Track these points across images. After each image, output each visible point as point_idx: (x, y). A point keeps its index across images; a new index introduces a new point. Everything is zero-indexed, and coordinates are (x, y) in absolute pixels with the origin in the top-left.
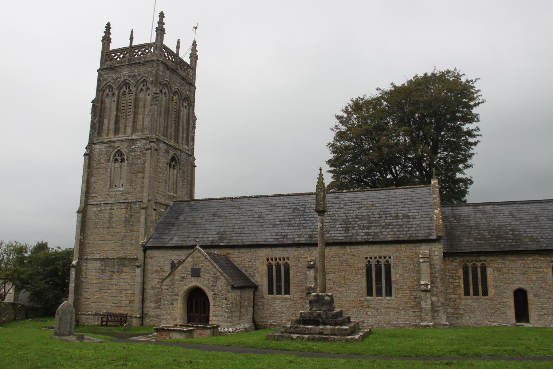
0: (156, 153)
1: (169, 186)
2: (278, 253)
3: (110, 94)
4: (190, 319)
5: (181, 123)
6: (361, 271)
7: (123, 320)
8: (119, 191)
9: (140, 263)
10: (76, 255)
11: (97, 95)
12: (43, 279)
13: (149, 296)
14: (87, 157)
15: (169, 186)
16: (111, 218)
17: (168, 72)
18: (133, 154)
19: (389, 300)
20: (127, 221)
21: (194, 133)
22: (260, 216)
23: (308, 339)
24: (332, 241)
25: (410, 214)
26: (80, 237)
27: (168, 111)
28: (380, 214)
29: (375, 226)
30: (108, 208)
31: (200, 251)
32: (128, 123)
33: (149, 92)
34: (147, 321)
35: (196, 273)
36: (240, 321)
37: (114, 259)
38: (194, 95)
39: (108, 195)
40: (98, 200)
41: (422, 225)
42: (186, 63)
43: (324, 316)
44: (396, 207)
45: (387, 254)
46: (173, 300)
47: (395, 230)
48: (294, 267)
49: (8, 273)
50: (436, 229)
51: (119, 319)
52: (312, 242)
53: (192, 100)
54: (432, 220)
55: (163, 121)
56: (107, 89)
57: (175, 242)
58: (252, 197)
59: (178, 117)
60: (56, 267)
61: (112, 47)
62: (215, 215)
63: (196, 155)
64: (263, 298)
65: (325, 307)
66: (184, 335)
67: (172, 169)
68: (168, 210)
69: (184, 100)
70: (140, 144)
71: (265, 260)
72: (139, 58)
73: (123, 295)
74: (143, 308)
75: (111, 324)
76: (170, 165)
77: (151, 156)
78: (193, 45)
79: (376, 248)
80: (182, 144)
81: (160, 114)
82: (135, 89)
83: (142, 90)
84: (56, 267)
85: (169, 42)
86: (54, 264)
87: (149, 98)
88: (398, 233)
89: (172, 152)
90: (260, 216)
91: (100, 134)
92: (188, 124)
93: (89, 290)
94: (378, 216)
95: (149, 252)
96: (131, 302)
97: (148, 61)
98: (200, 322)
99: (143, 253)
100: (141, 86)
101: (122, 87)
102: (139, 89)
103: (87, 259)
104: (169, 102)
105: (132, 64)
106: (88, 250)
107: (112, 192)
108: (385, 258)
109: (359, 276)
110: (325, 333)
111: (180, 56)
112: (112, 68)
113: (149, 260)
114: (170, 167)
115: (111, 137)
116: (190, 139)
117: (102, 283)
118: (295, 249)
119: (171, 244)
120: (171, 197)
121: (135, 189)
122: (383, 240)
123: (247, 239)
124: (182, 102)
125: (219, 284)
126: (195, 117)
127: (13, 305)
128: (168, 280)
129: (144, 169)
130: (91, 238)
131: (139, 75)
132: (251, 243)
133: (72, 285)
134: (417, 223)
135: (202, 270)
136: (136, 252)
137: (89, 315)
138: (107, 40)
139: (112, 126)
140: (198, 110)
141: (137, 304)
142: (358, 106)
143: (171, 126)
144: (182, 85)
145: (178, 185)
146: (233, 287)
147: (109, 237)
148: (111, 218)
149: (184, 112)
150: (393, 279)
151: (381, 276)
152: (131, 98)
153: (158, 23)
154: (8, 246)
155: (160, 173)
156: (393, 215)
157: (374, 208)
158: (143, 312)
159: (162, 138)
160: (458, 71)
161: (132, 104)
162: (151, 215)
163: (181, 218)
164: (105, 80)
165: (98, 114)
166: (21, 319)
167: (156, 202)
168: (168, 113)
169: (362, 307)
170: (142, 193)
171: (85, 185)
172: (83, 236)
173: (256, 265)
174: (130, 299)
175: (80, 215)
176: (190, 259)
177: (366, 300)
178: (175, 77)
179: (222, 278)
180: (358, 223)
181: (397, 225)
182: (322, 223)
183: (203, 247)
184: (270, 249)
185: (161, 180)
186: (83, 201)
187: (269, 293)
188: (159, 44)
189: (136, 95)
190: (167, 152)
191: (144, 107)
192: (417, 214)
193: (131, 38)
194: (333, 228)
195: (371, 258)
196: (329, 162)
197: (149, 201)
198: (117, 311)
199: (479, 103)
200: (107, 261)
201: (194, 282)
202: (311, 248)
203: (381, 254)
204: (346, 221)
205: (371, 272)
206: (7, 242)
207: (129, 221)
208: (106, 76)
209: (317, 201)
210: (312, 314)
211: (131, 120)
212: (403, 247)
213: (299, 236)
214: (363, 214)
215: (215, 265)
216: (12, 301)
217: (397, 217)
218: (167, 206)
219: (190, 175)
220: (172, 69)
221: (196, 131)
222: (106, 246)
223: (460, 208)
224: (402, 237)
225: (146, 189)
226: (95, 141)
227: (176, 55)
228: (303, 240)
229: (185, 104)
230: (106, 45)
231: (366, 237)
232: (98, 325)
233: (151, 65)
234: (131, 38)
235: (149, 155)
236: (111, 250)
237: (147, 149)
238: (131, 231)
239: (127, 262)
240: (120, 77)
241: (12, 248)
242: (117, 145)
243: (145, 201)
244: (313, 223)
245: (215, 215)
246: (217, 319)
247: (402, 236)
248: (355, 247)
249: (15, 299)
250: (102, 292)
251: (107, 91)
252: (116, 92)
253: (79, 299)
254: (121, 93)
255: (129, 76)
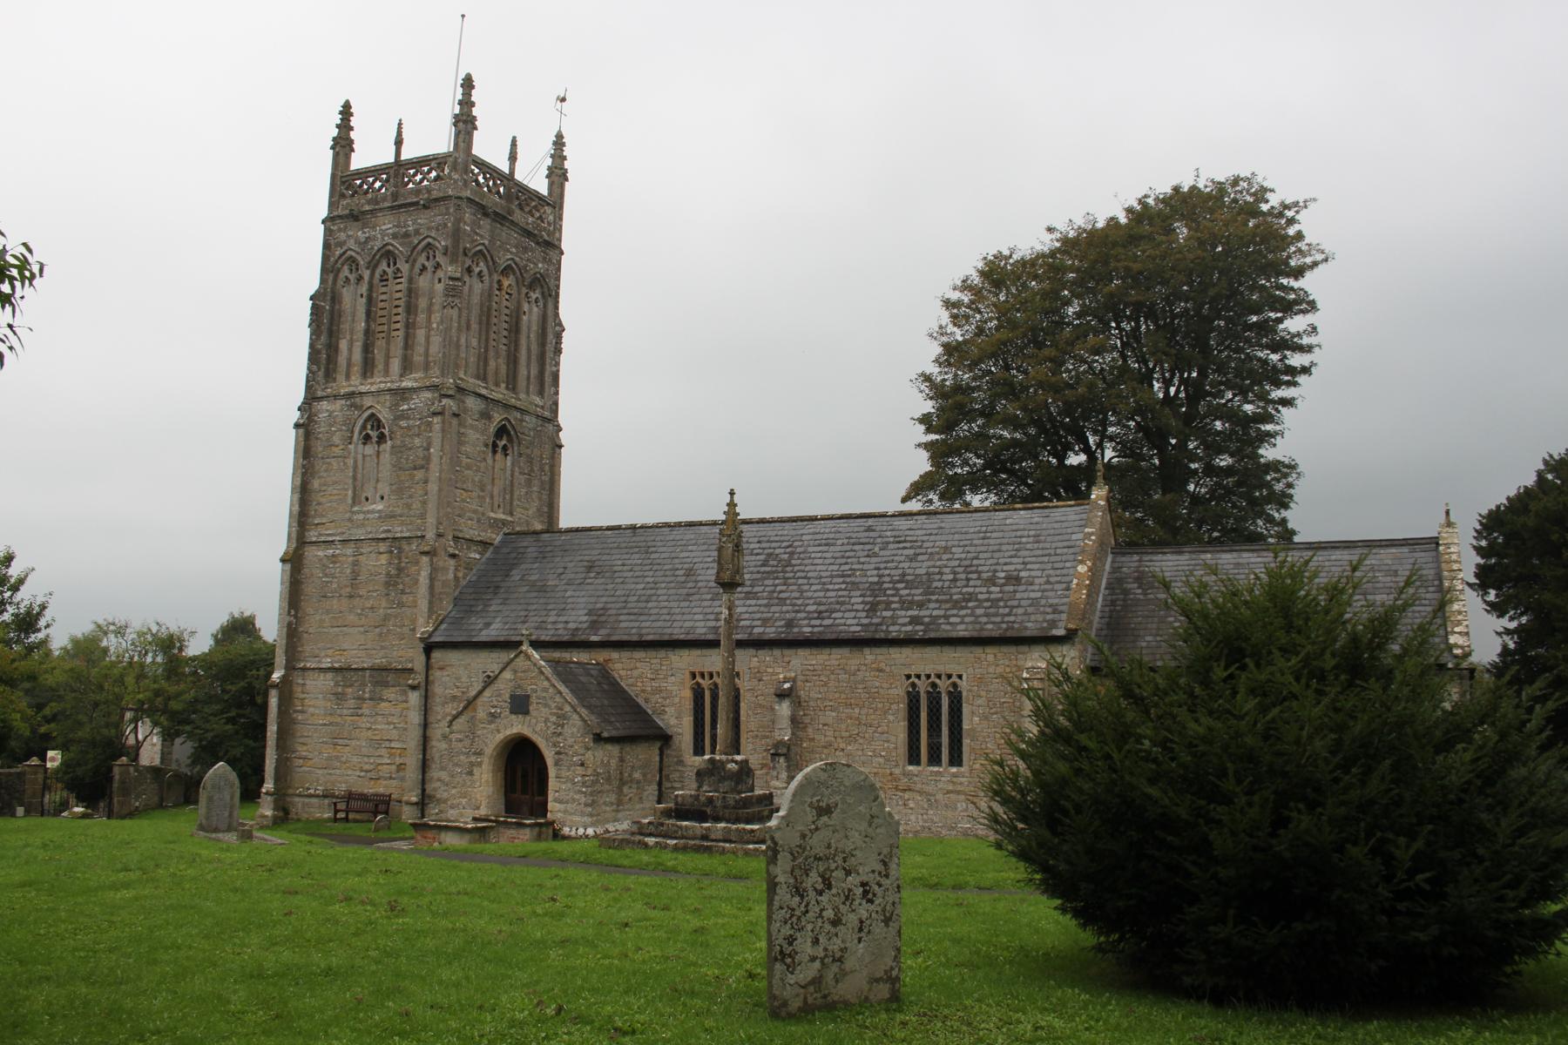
0: (455, 421)
1: (492, 497)
2: (713, 661)
3: (352, 277)
4: (511, 807)
5: (523, 341)
6: (894, 707)
7: (382, 807)
8: (372, 512)
9: (419, 679)
10: (280, 659)
11: (323, 281)
12: (222, 712)
13: (437, 756)
14: (301, 431)
15: (492, 497)
16: (355, 575)
17: (486, 223)
18: (403, 423)
19: (955, 775)
20: (390, 583)
21: (558, 364)
22: (689, 573)
23: (676, 848)
24: (833, 636)
25: (1023, 574)
26: (288, 619)
27: (489, 317)
28: (955, 573)
29: (937, 601)
30: (349, 551)
31: (528, 657)
32: (392, 348)
33: (440, 274)
34: (433, 810)
35: (520, 705)
36: (620, 815)
37: (363, 669)
38: (559, 269)
39: (350, 520)
40: (329, 532)
41: (1043, 602)
42: (536, 195)
43: (719, 803)
44: (996, 555)
45: (953, 669)
46: (472, 764)
47: (979, 611)
48: (748, 695)
49: (141, 696)
50: (1069, 613)
51: (370, 806)
52: (790, 637)
53: (552, 283)
54: (1068, 589)
55: (474, 342)
56: (346, 267)
57: (493, 632)
58: (679, 525)
59: (515, 329)
60: (250, 684)
61: (358, 162)
62: (590, 568)
63: (562, 419)
64: (681, 762)
65: (727, 785)
66: (467, 837)
67: (499, 456)
68: (488, 555)
69: (531, 287)
70: (420, 401)
71: (688, 676)
72: (417, 192)
73: (383, 752)
74: (423, 782)
75: (358, 816)
76: (495, 445)
77: (443, 430)
78: (555, 143)
79: (931, 652)
80: (528, 393)
81: (468, 327)
82: (407, 266)
83: (424, 268)
84: (250, 684)
85: (489, 147)
86: (245, 677)
87: (439, 287)
88: (984, 620)
89: (498, 417)
90: (689, 573)
91: (330, 375)
92: (543, 344)
93: (308, 740)
94: (951, 577)
95: (437, 655)
96: (401, 767)
97: (436, 200)
98: (532, 814)
99: (423, 658)
100: (422, 260)
101: (379, 262)
102: (418, 266)
103: (304, 669)
104: (490, 296)
105: (399, 206)
106: (307, 648)
107: (358, 512)
108: (949, 676)
109: (891, 718)
110: (713, 836)
111: (518, 176)
112: (355, 217)
113: (438, 674)
114: (495, 452)
115: (356, 383)
116: (547, 381)
117: (337, 724)
118: (752, 651)
119: (484, 636)
120: (497, 524)
121: (409, 506)
122: (945, 635)
123: (650, 629)
124: (524, 290)
125: (568, 731)
126: (560, 324)
127: (155, 771)
128: (462, 720)
129: (428, 459)
130: (315, 619)
131: (417, 232)
132: (657, 638)
133: (272, 729)
134: (1033, 595)
135: (533, 699)
136: (410, 653)
137: (311, 796)
138: (343, 145)
139: (357, 356)
140: (569, 307)
141: (412, 773)
142: (996, 273)
143: (497, 352)
144: (526, 249)
145: (516, 493)
146: (598, 738)
147: (352, 618)
148: (355, 575)
149: (531, 315)
150: (966, 726)
151: (939, 719)
152: (399, 287)
153: (460, 103)
154: (141, 634)
155: (468, 467)
156: (984, 576)
157: (945, 557)
158: (424, 790)
159: (472, 382)
160: (1260, 179)
161: (401, 303)
162: (446, 569)
163: (516, 575)
164: (341, 244)
165: (324, 328)
166: (175, 806)
167: (456, 538)
168: (488, 323)
169: (897, 788)
170: (423, 516)
171: (297, 496)
172: (296, 617)
173: (666, 687)
174: (398, 761)
175: (288, 567)
176: (507, 675)
177: (905, 774)
178: (505, 233)
179: (575, 717)
180: (903, 592)
181: (987, 600)
182: (730, 609)
183: (536, 645)
184: (699, 652)
185: (469, 486)
186: (294, 535)
187: (696, 753)
188: (461, 157)
189: (410, 280)
190: (485, 415)
191: (430, 311)
192: (1039, 573)
193: (399, 142)
194: (843, 603)
195: (918, 677)
196: (925, 420)
197: (440, 535)
198: (370, 789)
199: (1315, 264)
200: (348, 675)
201: (516, 726)
202: (787, 652)
203: (941, 669)
204: (876, 588)
205: (918, 709)
206: (137, 624)
207: (396, 581)
208: (342, 236)
209: (719, 563)
210: (696, 798)
211: (400, 342)
212: (990, 653)
213: (765, 622)
214: (918, 571)
215: (562, 688)
216: (157, 762)
217: (992, 581)
218: (485, 544)
219: (547, 468)
220: (496, 213)
221: (563, 358)
222: (346, 639)
223: (1160, 557)
224: (990, 630)
225: (432, 506)
226: (320, 394)
227: (509, 179)
228: (771, 632)
229: (534, 296)
230: (342, 159)
231: (909, 628)
232: (329, 820)
233: (443, 209)
234: (399, 142)
235: (437, 427)
236: (357, 648)
237: (435, 414)
238: (401, 605)
239: (391, 678)
240: (374, 238)
241: (149, 638)
242: (368, 401)
243: (430, 535)
244: (802, 592)
245: (590, 568)
246: (562, 807)
247: (990, 626)
248: (884, 650)
249: (162, 759)
250: (338, 742)
251: (345, 271)
252: (366, 274)
253: (288, 759)
254: (377, 276)
255: (395, 236)
